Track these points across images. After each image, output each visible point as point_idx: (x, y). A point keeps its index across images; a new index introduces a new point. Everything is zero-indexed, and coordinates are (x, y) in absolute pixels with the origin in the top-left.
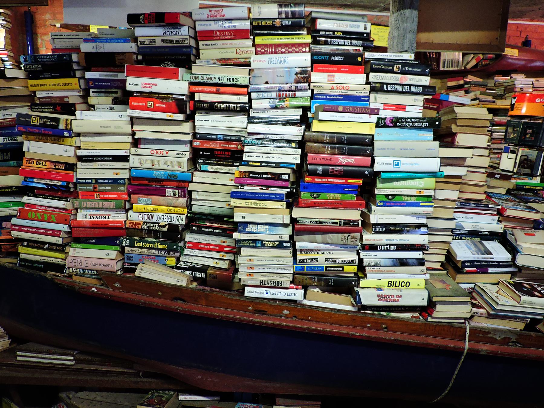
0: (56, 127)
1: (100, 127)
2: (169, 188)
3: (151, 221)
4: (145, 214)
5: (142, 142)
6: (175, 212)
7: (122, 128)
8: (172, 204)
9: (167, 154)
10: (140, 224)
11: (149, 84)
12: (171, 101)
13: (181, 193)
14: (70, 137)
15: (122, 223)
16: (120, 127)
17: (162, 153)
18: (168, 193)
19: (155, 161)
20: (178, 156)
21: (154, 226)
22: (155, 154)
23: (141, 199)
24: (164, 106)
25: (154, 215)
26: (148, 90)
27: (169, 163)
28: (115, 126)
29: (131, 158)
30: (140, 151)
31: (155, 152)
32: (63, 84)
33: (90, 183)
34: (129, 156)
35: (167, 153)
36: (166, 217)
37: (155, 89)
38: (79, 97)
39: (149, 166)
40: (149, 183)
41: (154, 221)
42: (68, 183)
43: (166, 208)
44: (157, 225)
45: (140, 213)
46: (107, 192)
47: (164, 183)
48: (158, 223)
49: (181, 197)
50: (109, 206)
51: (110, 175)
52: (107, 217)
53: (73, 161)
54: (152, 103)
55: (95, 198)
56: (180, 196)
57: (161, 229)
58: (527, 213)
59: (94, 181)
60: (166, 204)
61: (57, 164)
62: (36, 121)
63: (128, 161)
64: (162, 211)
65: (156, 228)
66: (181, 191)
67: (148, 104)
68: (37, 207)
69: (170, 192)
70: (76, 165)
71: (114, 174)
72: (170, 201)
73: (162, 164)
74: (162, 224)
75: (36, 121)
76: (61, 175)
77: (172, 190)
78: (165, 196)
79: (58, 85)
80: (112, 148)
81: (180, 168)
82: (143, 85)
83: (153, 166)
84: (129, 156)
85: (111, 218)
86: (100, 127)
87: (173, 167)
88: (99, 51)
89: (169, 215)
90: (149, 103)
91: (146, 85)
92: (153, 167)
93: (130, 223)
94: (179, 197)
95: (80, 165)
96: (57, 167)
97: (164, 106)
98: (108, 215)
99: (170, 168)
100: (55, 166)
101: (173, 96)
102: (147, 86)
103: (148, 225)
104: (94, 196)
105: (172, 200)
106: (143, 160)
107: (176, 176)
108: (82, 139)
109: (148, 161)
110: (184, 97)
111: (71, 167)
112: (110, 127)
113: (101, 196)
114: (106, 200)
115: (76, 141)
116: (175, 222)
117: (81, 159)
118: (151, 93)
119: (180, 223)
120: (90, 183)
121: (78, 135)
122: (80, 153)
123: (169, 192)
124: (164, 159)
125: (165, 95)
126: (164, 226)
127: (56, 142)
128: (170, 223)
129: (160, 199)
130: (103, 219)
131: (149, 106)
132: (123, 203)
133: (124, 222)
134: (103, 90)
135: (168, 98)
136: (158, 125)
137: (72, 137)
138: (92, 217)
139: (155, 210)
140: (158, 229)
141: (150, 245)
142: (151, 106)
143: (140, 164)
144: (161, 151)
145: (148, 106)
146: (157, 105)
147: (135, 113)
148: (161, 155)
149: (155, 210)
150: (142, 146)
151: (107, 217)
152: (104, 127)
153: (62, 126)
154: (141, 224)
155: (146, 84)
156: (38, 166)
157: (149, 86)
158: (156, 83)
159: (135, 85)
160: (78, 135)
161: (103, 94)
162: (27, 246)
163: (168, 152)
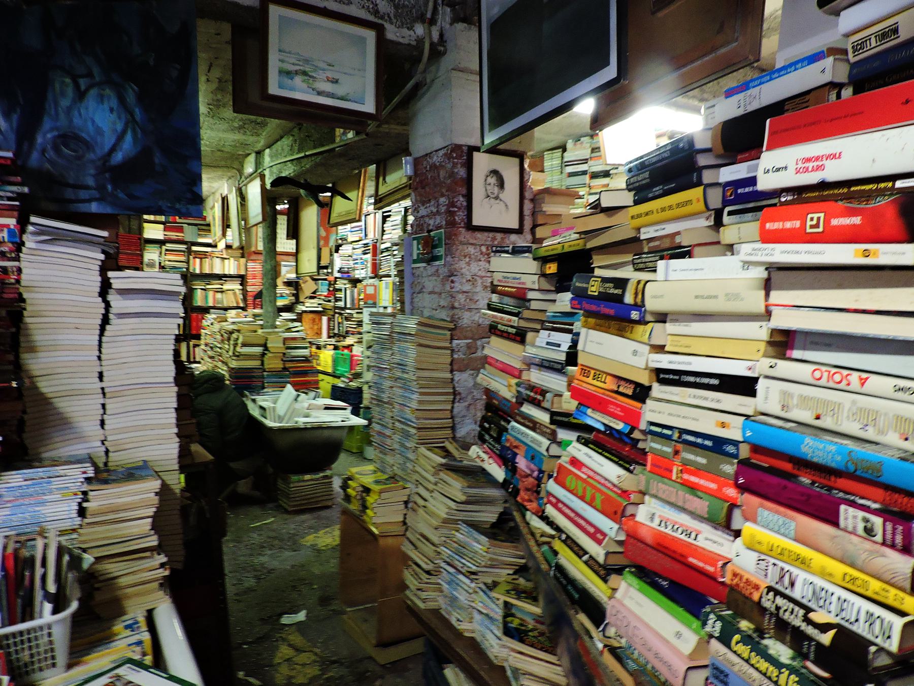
0: (619, 299)
1: (697, 297)
2: (853, 504)
3: (788, 592)
4: (774, 564)
5: (798, 340)
6: (869, 593)
7: (742, 300)
8: (859, 563)
9: (863, 384)
10: (757, 587)
11: (817, 159)
12: (882, 201)
13: (894, 534)
14: (642, 322)
15: (715, 566)
16: (736, 297)
17: (844, 382)
18: (846, 519)
19: (826, 403)
20: (900, 395)
21: (792, 613)
22: (823, 382)
23: (768, 513)
24: (857, 220)
25: (801, 576)
26: (812, 178)
27: (870, 417)
28: (727, 295)
29: (761, 386)
30: (784, 368)
31: (826, 374)
32: (678, 205)
33: (668, 438)
34: (756, 380)
35: (863, 382)
36: (834, 599)
37: (833, 172)
38: (707, 229)
39: (806, 416)
40: (795, 472)
41: (797, 594)
42: (633, 429)
43: (839, 569)
44: (802, 612)
45: (763, 557)
46: (698, 471)
47: (842, 482)
48: (808, 610)
49: (893, 546)
50: (696, 508)
51: (708, 424)
52: (693, 536)
53: (644, 379)
54: (819, 218)
55: (674, 477)
56: (889, 542)
57: (810, 630)
58: (875, 133)
59: (676, 436)
60: (839, 554)
61: (622, 383)
62: (593, 289)
63: (752, 393)
64: (826, 575)
65: (797, 622)
66: (894, 529)
67: (809, 223)
68: (584, 469)
69: (855, 517)
70: (649, 388)
71: (717, 425)
72: (850, 548)
73: (845, 415)
74: (819, 617)
75: (593, 289)
76: (623, 409)
77: (861, 514)
78: (835, 523)
79: (670, 207)
80: (723, 353)
81: (906, 439)
82: (800, 165)
83: (818, 418)
84: (756, 380)
85: (701, 542)
86: (697, 297)
87: (881, 432)
88: (750, 109)
89: (845, 595)
90: (812, 219)
91: (806, 165)
92: (817, 423)
93: (735, 575)
94: (884, 544)
95: (658, 390)
96: (621, 389)
97: (857, 220)
98: (696, 530)
99: (870, 434)
100: (619, 387)
101: (899, 184)
102: (810, 165)
103: (780, 601)
104: (671, 471)
105: (860, 547)
106: (791, 396)
107: (878, 467)
108: (670, 327)
109: (804, 399)
110: (131, 98)
111: (641, 393)
112: (716, 297)
113: (686, 476)
114: (693, 488)
115: (662, 333)
116: (861, 629)
117: (667, 377)
118: (823, 185)
119: (879, 641)
120: (668, 438)
121: (662, 318)
122: (664, 361)
123: (849, 515)
124: (854, 402)
125: (870, 186)
126: (824, 628)
127: (621, 333)
128: (843, 623)
129: (823, 529)
130: (683, 537)
131: (812, 227)
132: (725, 510)
133: (720, 563)
134: (751, 205)
135: (869, 196)
136: (841, 286)
137: (647, 323)
138: (663, 524)
139: (802, 563)
140: (804, 626)
141: (767, 669)
142: (817, 226)
143: (783, 406)
144: (845, 372)
145: (808, 227)
146: (835, 222)
147: (760, 253)
148: (843, 386)
149: (802, 563)
150: (796, 354)
151: (693, 536)
152: (702, 297)
153: (629, 299)
154: (761, 590)
155: (809, 160)
156: (595, 382)
157: (815, 164)
158: (836, 151)
159: (778, 170)
160: (662, 318)
161: (750, 214)
162: (564, 542)
163: (867, 378)
